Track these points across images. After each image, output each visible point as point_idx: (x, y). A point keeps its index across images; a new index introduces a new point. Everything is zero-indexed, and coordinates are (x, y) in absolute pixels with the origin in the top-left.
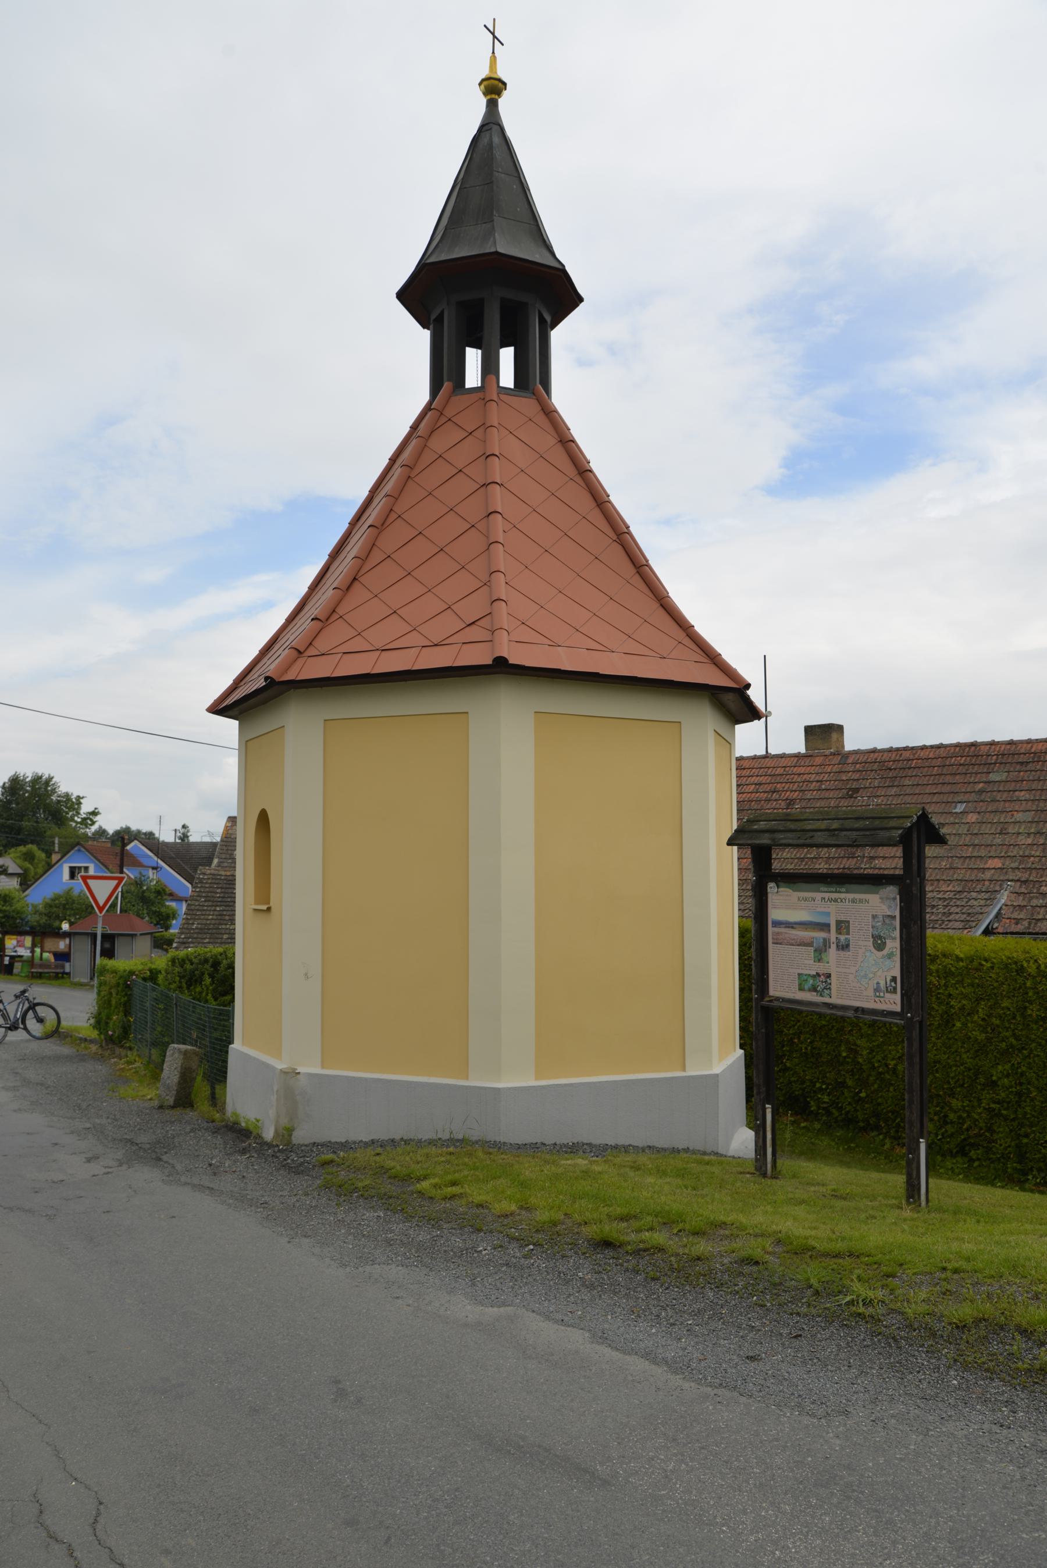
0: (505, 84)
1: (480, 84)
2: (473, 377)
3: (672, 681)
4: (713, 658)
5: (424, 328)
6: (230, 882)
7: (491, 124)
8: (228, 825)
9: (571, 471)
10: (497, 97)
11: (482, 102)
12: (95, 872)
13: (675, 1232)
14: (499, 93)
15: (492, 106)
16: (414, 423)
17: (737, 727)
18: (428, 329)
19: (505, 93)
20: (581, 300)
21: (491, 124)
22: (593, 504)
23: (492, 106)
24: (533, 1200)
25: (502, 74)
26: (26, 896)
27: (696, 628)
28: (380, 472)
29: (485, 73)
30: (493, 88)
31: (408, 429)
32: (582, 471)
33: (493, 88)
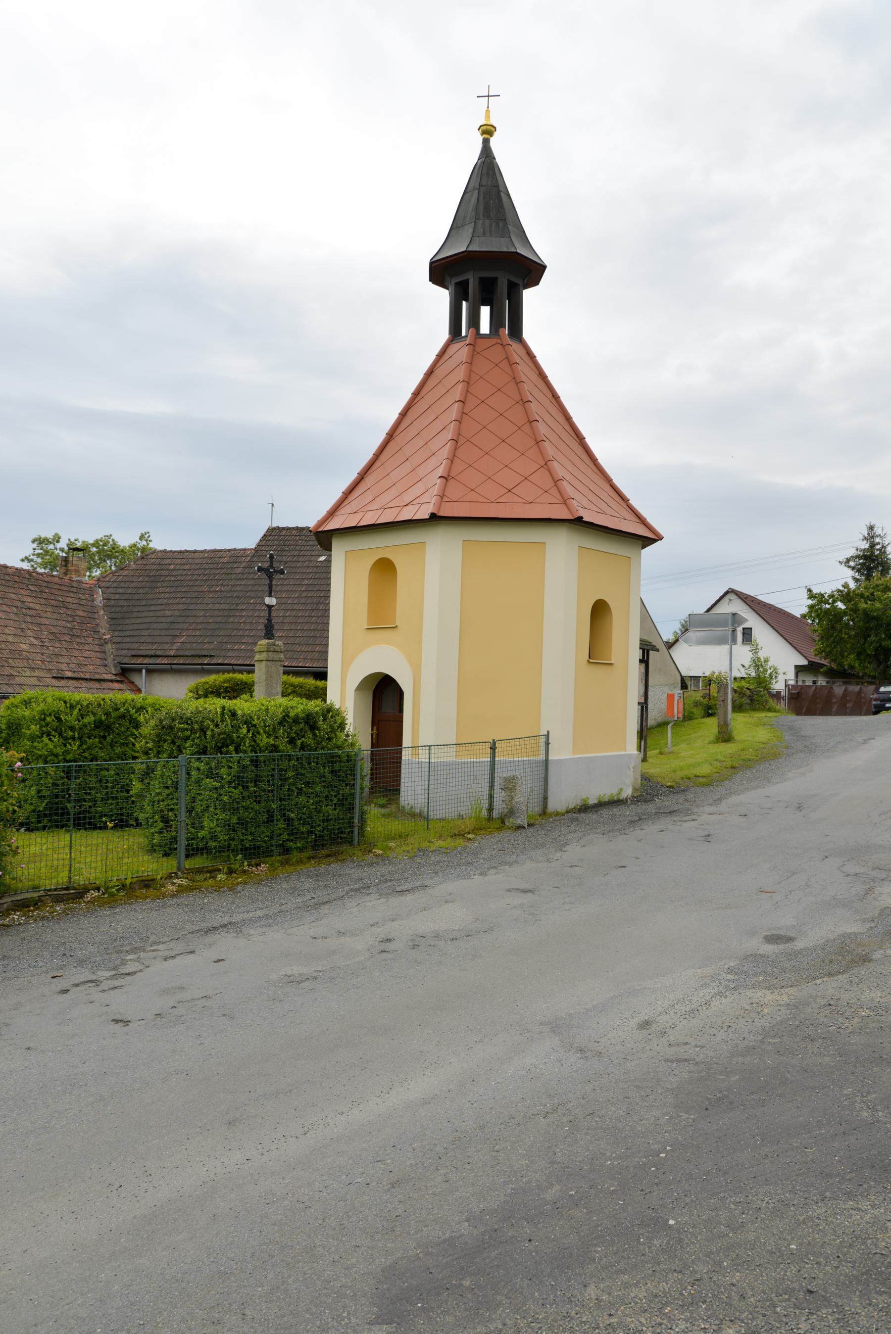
0: (495, 128)
1: (479, 129)
2: (485, 327)
3: (593, 523)
7: (487, 153)
9: (550, 396)
10: (489, 137)
11: (479, 139)
12: (574, 753)
13: (589, 1053)
17: (643, 551)
18: (447, 288)
19: (496, 134)
20: (543, 268)
21: (487, 153)
23: (486, 143)
24: (246, 1312)
25: (493, 122)
26: (703, 723)
27: (614, 481)
28: (790, 612)
30: (488, 131)
32: (555, 397)
33: (488, 131)
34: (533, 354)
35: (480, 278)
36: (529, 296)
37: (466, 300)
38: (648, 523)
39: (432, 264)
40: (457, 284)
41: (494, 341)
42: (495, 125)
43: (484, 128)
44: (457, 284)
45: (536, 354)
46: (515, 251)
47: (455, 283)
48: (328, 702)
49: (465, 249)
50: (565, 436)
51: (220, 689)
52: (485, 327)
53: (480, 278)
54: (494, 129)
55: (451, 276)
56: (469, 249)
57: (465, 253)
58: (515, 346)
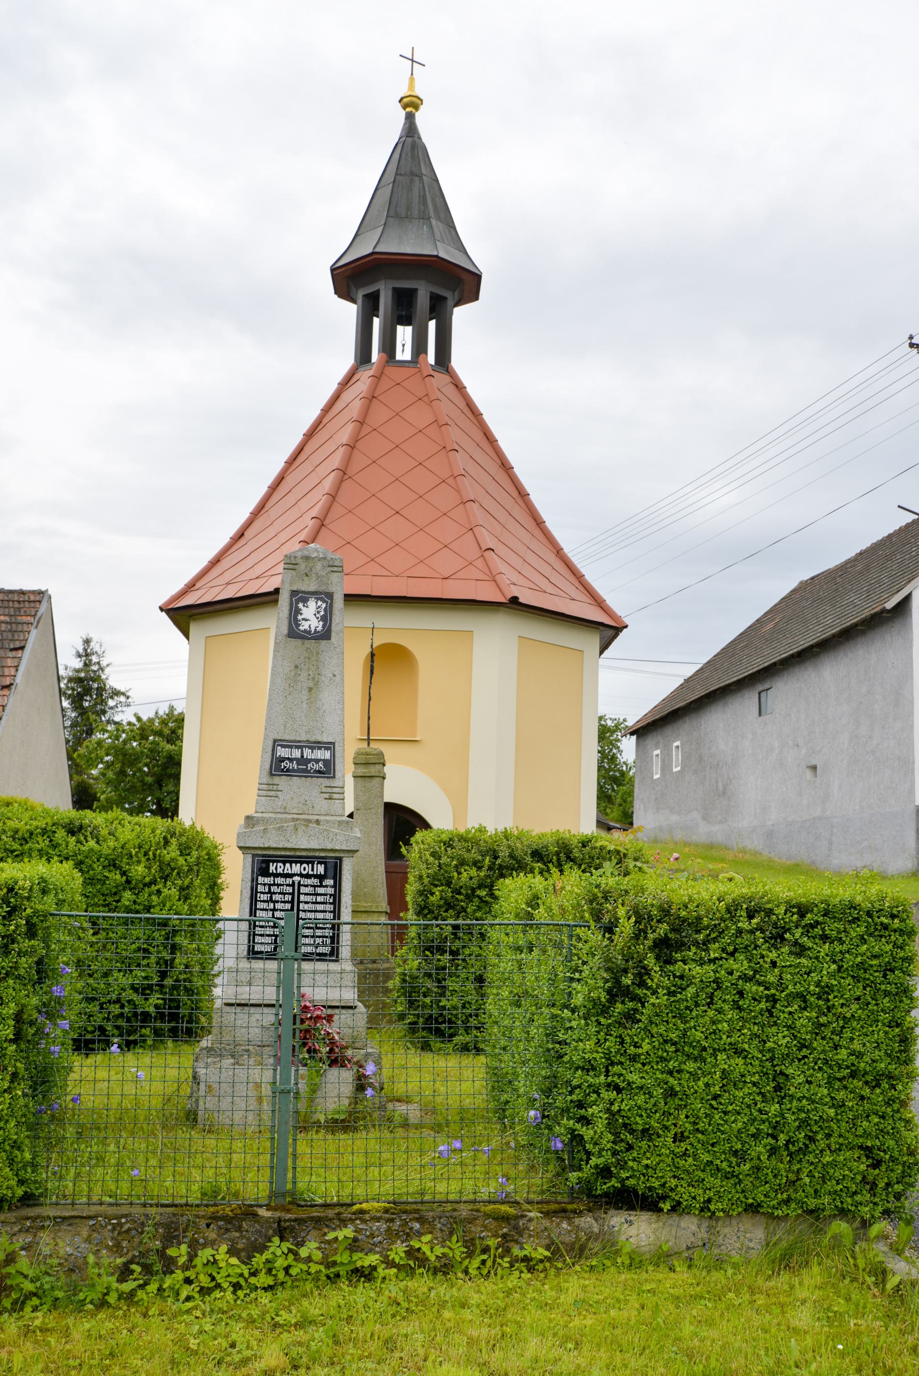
0: (421, 100)
1: (400, 101)
2: (404, 353)
4: (599, 602)
5: (336, 293)
6: (290, 566)
7: (410, 130)
8: (180, 731)
9: (515, 493)
10: (414, 111)
14: (417, 108)
15: (410, 118)
16: (309, 430)
18: (353, 301)
19: (422, 108)
21: (410, 130)
22: (535, 524)
23: (410, 118)
25: (418, 92)
27: (484, 416)
29: (404, 91)
30: (411, 104)
31: (283, 464)
32: (506, 466)
33: (411, 104)
34: (479, 410)
35: (394, 289)
36: (461, 315)
37: (378, 317)
38: (607, 605)
39: (333, 270)
40: (366, 296)
41: (412, 371)
42: (421, 97)
43: (405, 100)
44: (366, 296)
45: (482, 411)
46: (435, 253)
47: (365, 296)
48: (187, 814)
49: (369, 250)
50: (509, 503)
51: (94, 681)
52: (404, 353)
53: (394, 289)
54: (419, 102)
55: (358, 287)
56: (377, 250)
57: (375, 256)
58: (441, 379)
